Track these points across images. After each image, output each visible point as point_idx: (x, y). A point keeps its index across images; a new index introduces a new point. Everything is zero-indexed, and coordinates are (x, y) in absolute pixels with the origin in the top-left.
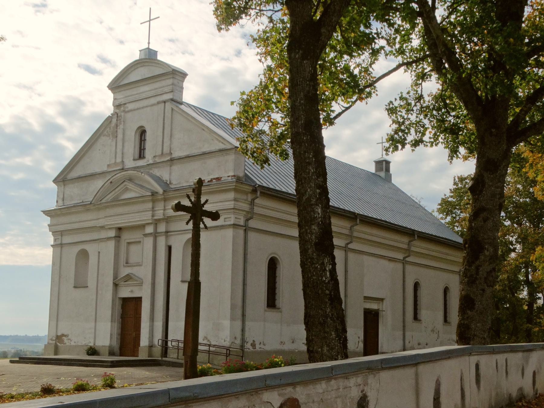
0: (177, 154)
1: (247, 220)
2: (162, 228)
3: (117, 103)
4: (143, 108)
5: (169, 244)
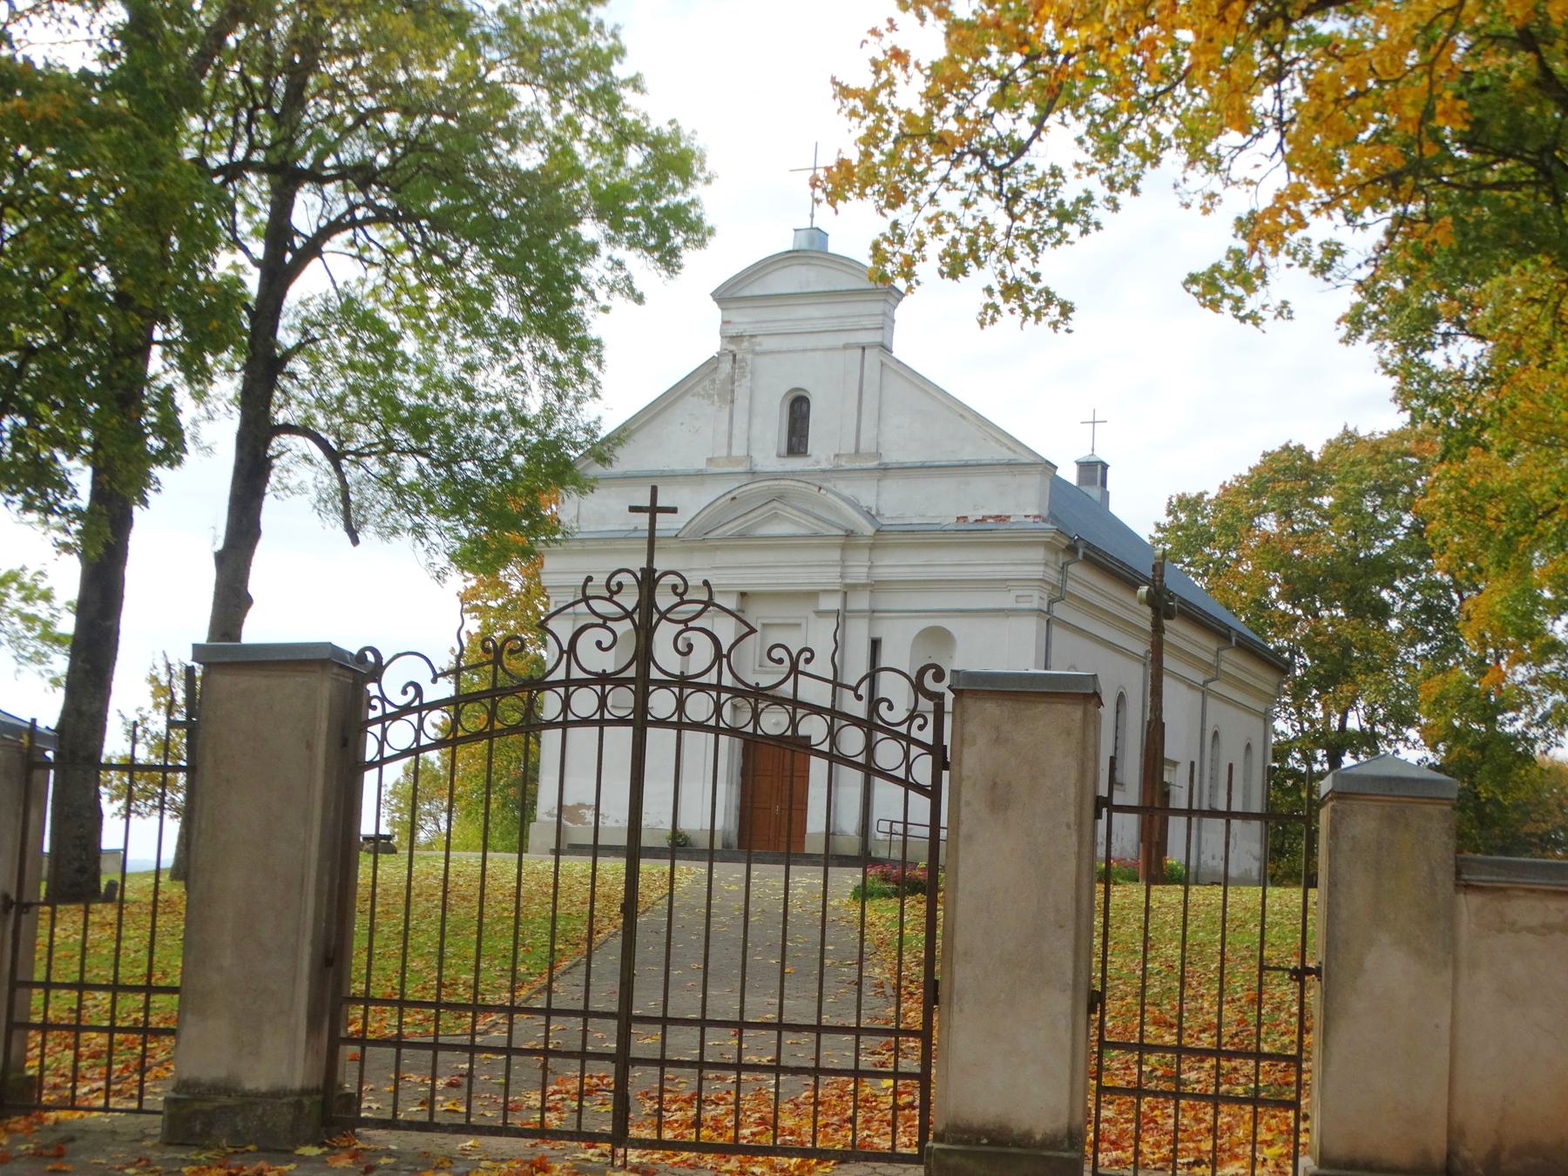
0: (893, 457)
1: (1051, 602)
2: (860, 602)
3: (733, 331)
4: (804, 351)
5: (877, 635)
